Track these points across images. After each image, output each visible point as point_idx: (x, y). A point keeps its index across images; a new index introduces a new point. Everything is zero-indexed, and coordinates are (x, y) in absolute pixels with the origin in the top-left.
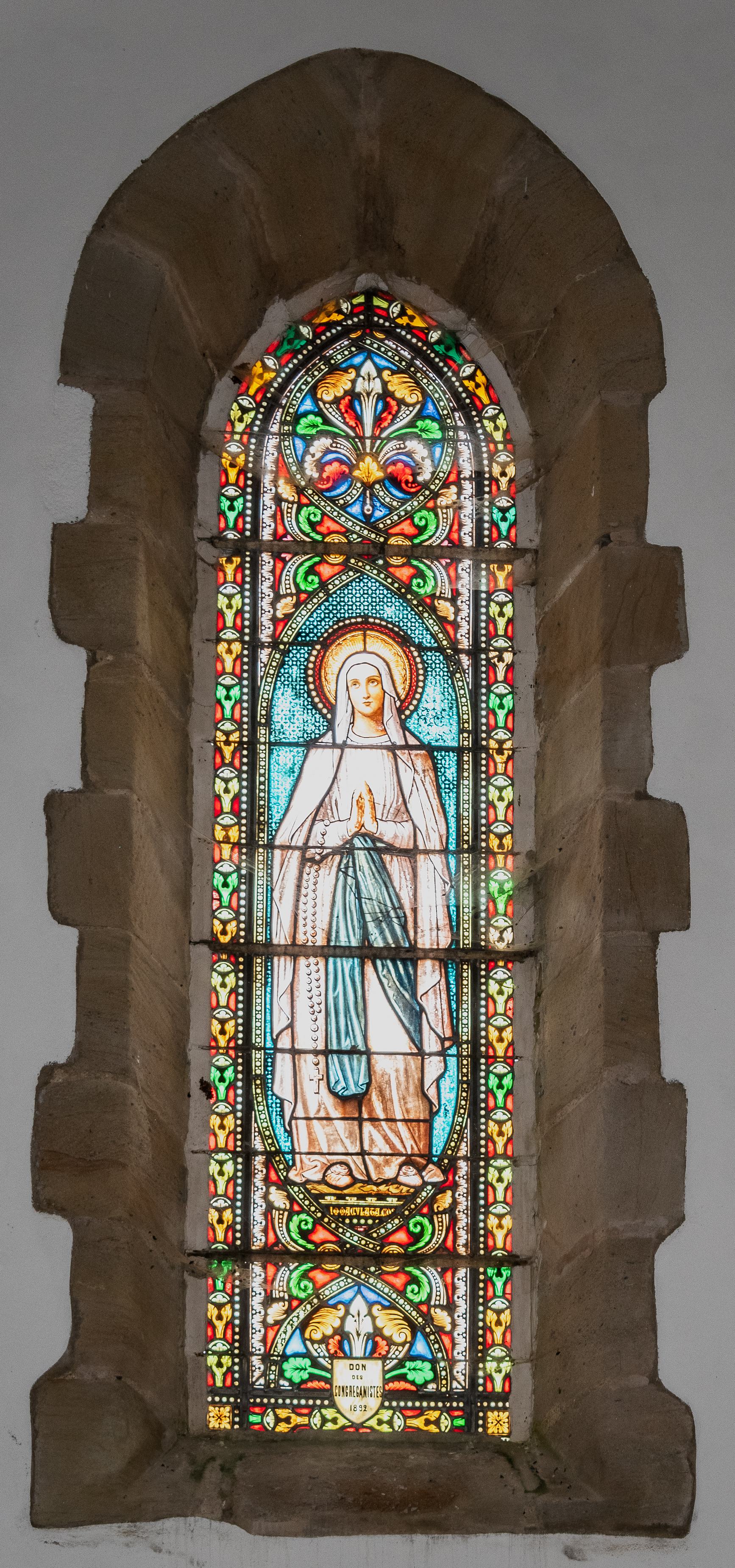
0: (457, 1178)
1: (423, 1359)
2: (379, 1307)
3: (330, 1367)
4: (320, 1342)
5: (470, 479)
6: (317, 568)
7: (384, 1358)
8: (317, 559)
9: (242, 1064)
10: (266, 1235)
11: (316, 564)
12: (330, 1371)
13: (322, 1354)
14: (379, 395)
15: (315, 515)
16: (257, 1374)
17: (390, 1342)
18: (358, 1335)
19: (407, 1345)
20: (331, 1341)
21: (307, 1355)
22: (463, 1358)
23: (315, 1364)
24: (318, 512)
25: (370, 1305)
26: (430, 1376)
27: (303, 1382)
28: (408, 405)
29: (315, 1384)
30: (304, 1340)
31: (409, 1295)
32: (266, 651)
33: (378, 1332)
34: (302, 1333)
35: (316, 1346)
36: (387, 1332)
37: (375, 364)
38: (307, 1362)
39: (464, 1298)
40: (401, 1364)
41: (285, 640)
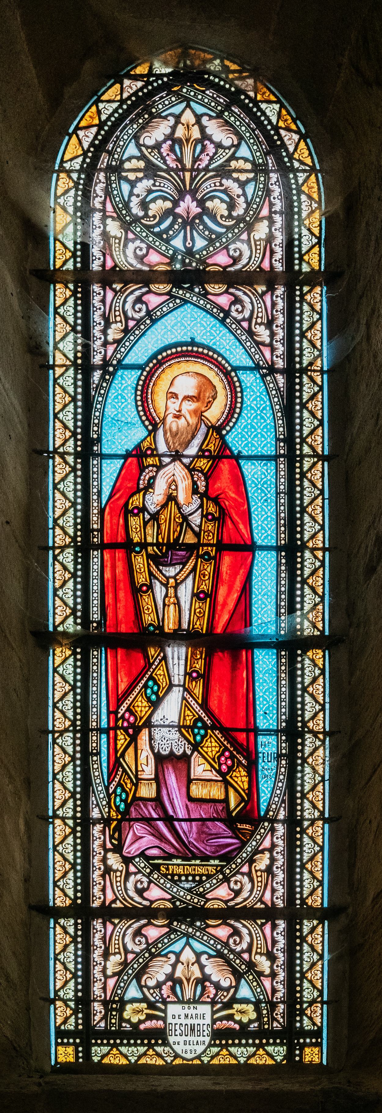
2: (207, 118)
5: (281, 213)
6: (144, 298)
9: (81, 977)
10: (104, 894)
11: (143, 294)
12: (165, 1011)
16: (97, 1018)
17: (217, 986)
18: (188, 980)
21: (145, 999)
23: (151, 1006)
24: (144, 246)
26: (253, 1016)
27: (140, 1022)
28: (224, 148)
29: (148, 1024)
30: (141, 987)
32: (99, 827)
34: (139, 982)
36: (214, 978)
37: (193, 112)
38: (144, 1005)
40: (228, 1005)
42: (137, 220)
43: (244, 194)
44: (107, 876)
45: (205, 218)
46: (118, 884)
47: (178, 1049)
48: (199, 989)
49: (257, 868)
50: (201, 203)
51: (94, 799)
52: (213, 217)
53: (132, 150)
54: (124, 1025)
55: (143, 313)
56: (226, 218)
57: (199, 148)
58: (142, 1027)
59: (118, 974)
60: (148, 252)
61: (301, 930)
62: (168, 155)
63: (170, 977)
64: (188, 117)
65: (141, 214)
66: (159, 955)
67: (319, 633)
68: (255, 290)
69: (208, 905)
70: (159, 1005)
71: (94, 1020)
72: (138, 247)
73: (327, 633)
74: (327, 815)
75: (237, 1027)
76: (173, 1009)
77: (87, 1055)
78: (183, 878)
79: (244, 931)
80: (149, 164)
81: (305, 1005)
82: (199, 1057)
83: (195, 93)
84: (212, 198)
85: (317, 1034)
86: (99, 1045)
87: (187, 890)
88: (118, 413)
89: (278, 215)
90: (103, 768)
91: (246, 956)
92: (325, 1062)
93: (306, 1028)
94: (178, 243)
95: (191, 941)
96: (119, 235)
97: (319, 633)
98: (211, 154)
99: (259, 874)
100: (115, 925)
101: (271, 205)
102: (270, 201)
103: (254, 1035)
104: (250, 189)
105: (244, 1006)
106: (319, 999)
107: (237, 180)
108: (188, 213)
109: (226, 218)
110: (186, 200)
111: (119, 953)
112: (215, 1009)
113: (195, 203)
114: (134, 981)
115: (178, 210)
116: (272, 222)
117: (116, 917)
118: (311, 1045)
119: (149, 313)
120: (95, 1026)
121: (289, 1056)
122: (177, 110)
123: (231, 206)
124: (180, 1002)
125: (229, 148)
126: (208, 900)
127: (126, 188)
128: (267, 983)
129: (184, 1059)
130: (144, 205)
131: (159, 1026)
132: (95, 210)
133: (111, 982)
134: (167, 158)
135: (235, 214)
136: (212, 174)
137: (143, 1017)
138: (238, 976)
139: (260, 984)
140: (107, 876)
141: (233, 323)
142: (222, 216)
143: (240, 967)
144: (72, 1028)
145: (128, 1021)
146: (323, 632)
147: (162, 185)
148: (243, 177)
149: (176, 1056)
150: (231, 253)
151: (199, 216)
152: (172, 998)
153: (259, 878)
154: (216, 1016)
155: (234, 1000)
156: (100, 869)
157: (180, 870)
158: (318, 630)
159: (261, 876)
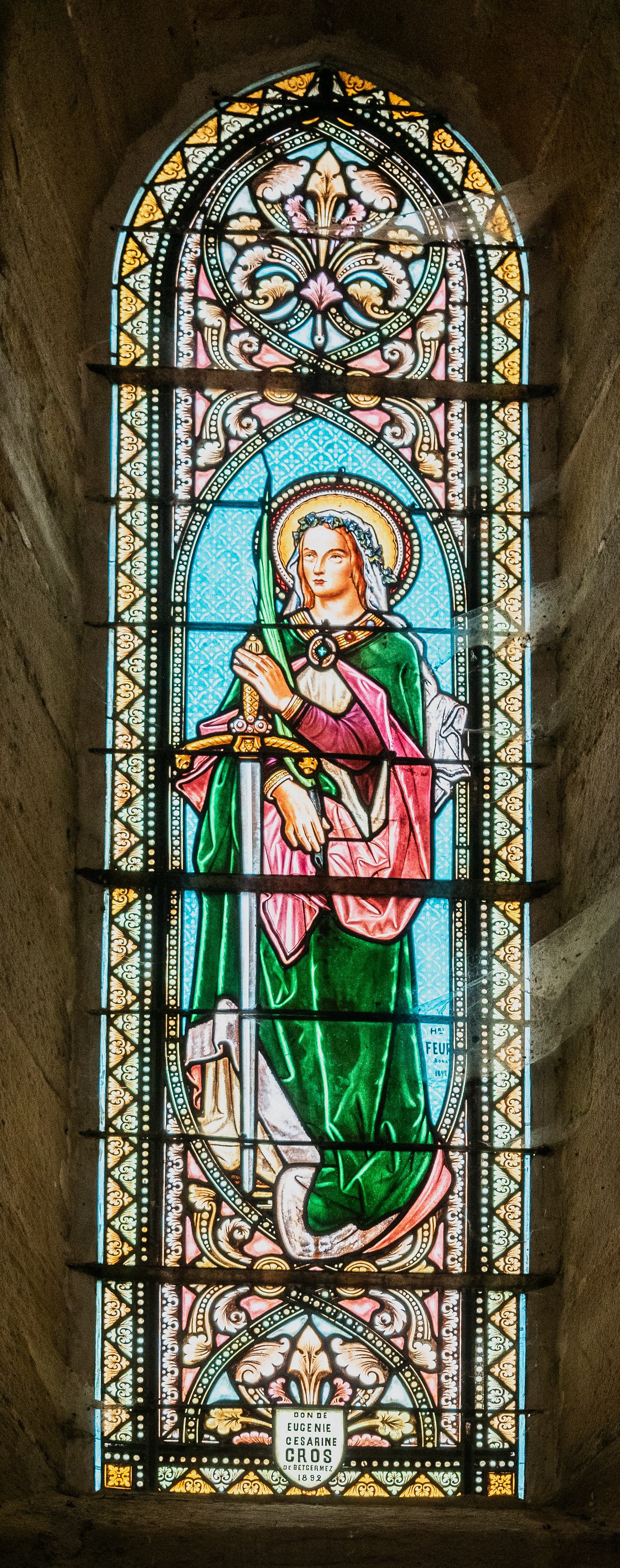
1: (400, 1408)
2: (354, 168)
3: (270, 1416)
4: (255, 1386)
5: (463, 304)
6: (254, 410)
10: (184, 1246)
12: (271, 1421)
13: (261, 1402)
16: (167, 1427)
17: (356, 1384)
20: (273, 1385)
21: (242, 1403)
25: (343, 165)
26: (409, 1429)
27: (232, 1434)
30: (235, 1385)
31: (379, 1327)
33: (337, 1372)
34: (232, 1377)
35: (251, 1391)
39: (461, 1259)
40: (369, 1413)
41: (209, 497)
43: (409, 278)
44: (188, 1218)
45: (346, 305)
46: (205, 1236)
47: (293, 1475)
50: (342, 287)
51: (169, 1106)
52: (359, 306)
55: (252, 431)
56: (380, 308)
57: (342, 209)
58: (236, 1440)
59: (200, 1364)
61: (484, 1305)
62: (296, 215)
64: (329, 164)
65: (247, 292)
66: (264, 1339)
70: (262, 1410)
71: (162, 1430)
72: (246, 342)
76: (284, 1417)
79: (398, 1307)
80: (266, 224)
82: (326, 1485)
84: (358, 280)
86: (170, 1465)
88: (208, 693)
89: (458, 308)
90: (185, 985)
91: (399, 1342)
93: (492, 1446)
94: (303, 336)
95: (316, 1319)
96: (217, 324)
98: (359, 218)
100: (198, 1295)
101: (449, 293)
104: (416, 269)
107: (398, 258)
108: (321, 298)
109: (380, 308)
110: (319, 279)
112: (350, 1417)
113: (332, 285)
114: (225, 1374)
115: (305, 292)
116: (448, 318)
117: (198, 1282)
118: (499, 1471)
119: (260, 429)
120: (165, 1437)
121: (467, 1485)
122: (312, 152)
123: (388, 292)
124: (295, 1405)
125: (387, 212)
128: (432, 1382)
129: (302, 1488)
130: (253, 282)
131: (261, 1440)
133: (189, 1377)
134: (294, 219)
136: (365, 245)
137: (237, 1427)
139: (423, 1386)
140: (188, 1218)
141: (388, 450)
142: (373, 306)
143: (391, 1360)
144: (128, 1439)
145: (214, 1432)
147: (283, 257)
148: (407, 253)
149: (291, 1484)
151: (338, 305)
152: (286, 1401)
154: (351, 1428)
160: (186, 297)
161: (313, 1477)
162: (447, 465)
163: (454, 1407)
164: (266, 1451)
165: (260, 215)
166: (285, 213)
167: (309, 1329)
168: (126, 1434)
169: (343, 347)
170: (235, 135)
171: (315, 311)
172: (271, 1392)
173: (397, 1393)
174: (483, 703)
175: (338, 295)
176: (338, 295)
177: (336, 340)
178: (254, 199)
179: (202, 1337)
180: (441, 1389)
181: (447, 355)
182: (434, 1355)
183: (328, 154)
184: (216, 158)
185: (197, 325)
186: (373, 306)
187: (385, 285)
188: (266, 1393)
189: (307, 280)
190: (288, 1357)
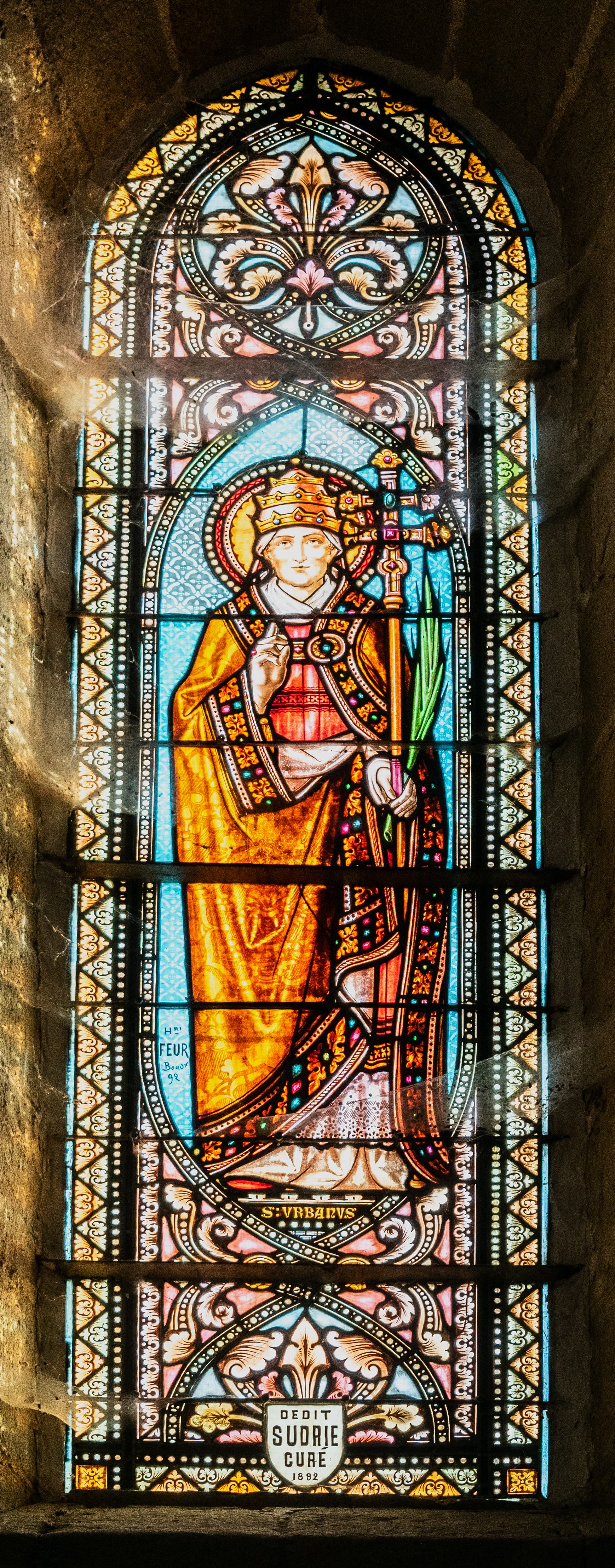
0: (450, 477)
7: (345, 1400)
8: (236, 386)
11: (235, 392)
12: (261, 1417)
14: (319, 1368)
15: (231, 336)
18: (305, 1369)
19: (384, 200)
22: (469, 1397)
26: (418, 1421)
27: (218, 1433)
28: (369, 199)
29: (235, 1436)
38: (228, 1407)
40: (371, 1407)
42: (222, 295)
43: (404, 259)
45: (337, 291)
47: (287, 1474)
48: (324, 1384)
49: (426, 1210)
50: (333, 274)
52: (353, 292)
53: (219, 200)
54: (190, 1434)
56: (377, 290)
57: (327, 200)
60: (242, 340)
62: (279, 207)
63: (273, 1365)
65: (229, 286)
67: (524, 865)
68: (414, 384)
69: (345, 1261)
70: (252, 1405)
71: (141, 1429)
73: (538, 866)
74: (545, 1130)
75: (391, 1439)
77: (129, 1479)
78: (307, 1225)
81: (510, 1408)
82: (325, 1483)
83: (326, 127)
84: (349, 268)
85: (533, 1449)
87: (310, 1242)
91: (407, 1335)
92: (545, 1492)
93: (513, 1442)
97: (524, 865)
98: (348, 207)
99: (429, 1217)
102: (445, 271)
103: (421, 1451)
105: (403, 1407)
106: (536, 1399)
111: (188, 1330)
112: (349, 1413)
123: (383, 275)
126: (343, 1256)
127: (206, 251)
130: (236, 275)
132: (157, 286)
133: (171, 1374)
134: (276, 212)
135: (388, 286)
138: (392, 1362)
139: (434, 1380)
142: (369, 291)
143: (394, 1349)
145: (199, 1430)
146: (531, 863)
149: (285, 1483)
150: (381, 339)
151: (328, 290)
153: (431, 1225)
154: (350, 1425)
155: (383, 1398)
156: (152, 1208)
157: (297, 1212)
158: (525, 860)
159: (433, 1221)
160: (162, 293)
161: (309, 1475)
162: (446, 445)
163: (469, 1397)
164: (258, 1450)
165: (239, 210)
166: (267, 206)
167: (304, 1321)
168: (99, 1434)
169: (334, 333)
170: (214, 134)
171: (301, 301)
172: (260, 1387)
173: (403, 1384)
174: (487, 695)
175: (329, 281)
176: (329, 281)
177: (327, 325)
178: (231, 196)
179: (185, 1334)
180: (455, 1379)
181: (161, 1315)
182: (446, 1345)
183: (312, 148)
184: (193, 158)
185: (175, 319)
186: (369, 291)
187: (379, 269)
188: (256, 1389)
189: (294, 269)
190: (280, 1351)
